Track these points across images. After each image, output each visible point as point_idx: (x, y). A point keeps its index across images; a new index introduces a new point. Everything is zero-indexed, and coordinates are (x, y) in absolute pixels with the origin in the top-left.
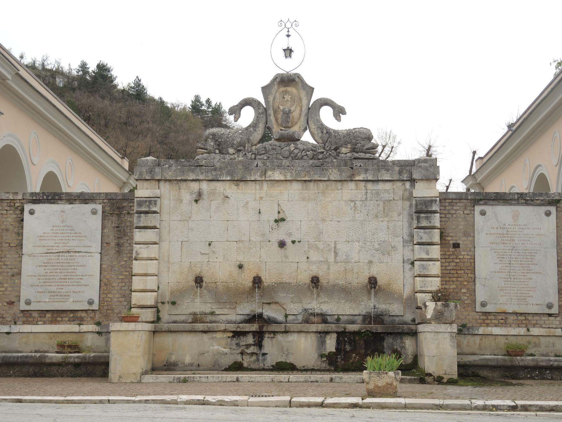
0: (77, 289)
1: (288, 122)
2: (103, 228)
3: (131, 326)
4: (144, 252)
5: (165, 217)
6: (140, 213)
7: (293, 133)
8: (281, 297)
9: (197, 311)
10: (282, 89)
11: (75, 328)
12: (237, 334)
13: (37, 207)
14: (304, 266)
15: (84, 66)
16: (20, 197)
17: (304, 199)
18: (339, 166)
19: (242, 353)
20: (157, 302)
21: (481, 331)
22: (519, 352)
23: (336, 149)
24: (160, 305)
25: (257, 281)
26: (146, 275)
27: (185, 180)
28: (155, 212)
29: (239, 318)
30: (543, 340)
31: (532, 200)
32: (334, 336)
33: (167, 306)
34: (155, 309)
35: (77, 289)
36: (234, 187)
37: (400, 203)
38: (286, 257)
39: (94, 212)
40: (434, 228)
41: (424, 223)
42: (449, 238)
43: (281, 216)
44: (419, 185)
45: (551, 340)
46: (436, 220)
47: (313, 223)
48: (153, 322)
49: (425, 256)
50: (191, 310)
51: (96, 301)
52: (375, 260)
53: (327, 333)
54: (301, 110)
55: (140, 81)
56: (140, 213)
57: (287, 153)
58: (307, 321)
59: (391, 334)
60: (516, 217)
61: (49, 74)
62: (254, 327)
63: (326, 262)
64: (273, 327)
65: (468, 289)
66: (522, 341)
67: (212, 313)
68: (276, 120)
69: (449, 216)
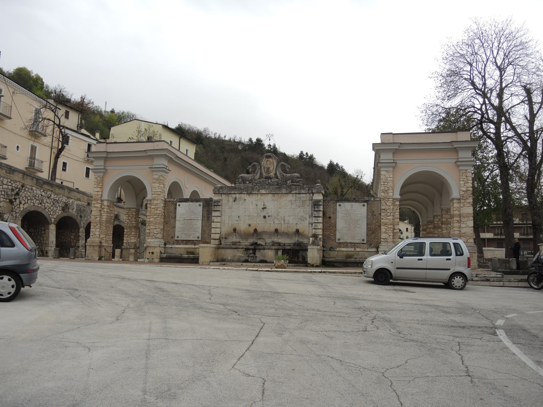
0: (194, 233)
1: (268, 172)
2: (203, 211)
3: (206, 245)
4: (215, 219)
5: (223, 207)
6: (214, 205)
7: (270, 176)
8: (264, 236)
9: (234, 241)
10: (267, 159)
11: (193, 246)
12: (247, 250)
13: (181, 204)
14: (272, 225)
15: (250, 140)
16: (175, 200)
17: (273, 200)
18: (286, 188)
19: (248, 256)
20: (220, 238)
21: (338, 249)
22: (350, 257)
23: (286, 181)
24: (221, 239)
25: (255, 230)
26: (216, 228)
27: (231, 194)
28: (220, 205)
29: (249, 244)
30: (360, 252)
31: (358, 201)
32: (281, 250)
33: (224, 239)
34: (219, 240)
35: (194, 233)
36: (248, 196)
37: (308, 202)
38: (266, 222)
39: (200, 205)
40: (320, 211)
41: (316, 209)
42: (327, 215)
43: (265, 207)
44: (315, 195)
45: (363, 253)
46: (321, 208)
47: (276, 209)
48: (218, 245)
49: (316, 221)
50: (232, 241)
51: (200, 237)
52: (298, 223)
53: (279, 249)
54: (274, 167)
55: (275, 145)
56: (214, 205)
57: (268, 183)
58: (273, 245)
59: (302, 250)
60: (352, 207)
61: (236, 144)
62: (253, 247)
63: (281, 223)
64: (259, 247)
65: (333, 234)
66: (352, 253)
67: (239, 242)
68: (264, 171)
69: (328, 206)
